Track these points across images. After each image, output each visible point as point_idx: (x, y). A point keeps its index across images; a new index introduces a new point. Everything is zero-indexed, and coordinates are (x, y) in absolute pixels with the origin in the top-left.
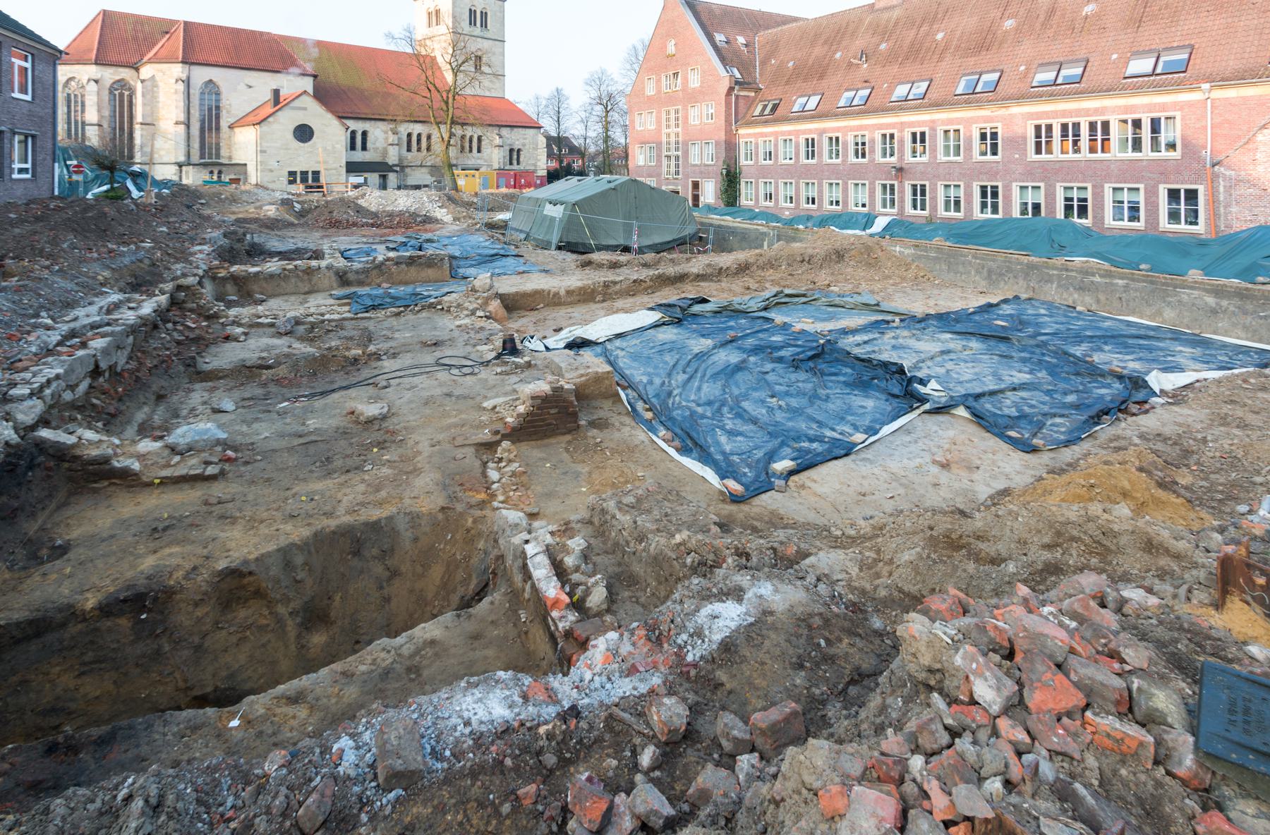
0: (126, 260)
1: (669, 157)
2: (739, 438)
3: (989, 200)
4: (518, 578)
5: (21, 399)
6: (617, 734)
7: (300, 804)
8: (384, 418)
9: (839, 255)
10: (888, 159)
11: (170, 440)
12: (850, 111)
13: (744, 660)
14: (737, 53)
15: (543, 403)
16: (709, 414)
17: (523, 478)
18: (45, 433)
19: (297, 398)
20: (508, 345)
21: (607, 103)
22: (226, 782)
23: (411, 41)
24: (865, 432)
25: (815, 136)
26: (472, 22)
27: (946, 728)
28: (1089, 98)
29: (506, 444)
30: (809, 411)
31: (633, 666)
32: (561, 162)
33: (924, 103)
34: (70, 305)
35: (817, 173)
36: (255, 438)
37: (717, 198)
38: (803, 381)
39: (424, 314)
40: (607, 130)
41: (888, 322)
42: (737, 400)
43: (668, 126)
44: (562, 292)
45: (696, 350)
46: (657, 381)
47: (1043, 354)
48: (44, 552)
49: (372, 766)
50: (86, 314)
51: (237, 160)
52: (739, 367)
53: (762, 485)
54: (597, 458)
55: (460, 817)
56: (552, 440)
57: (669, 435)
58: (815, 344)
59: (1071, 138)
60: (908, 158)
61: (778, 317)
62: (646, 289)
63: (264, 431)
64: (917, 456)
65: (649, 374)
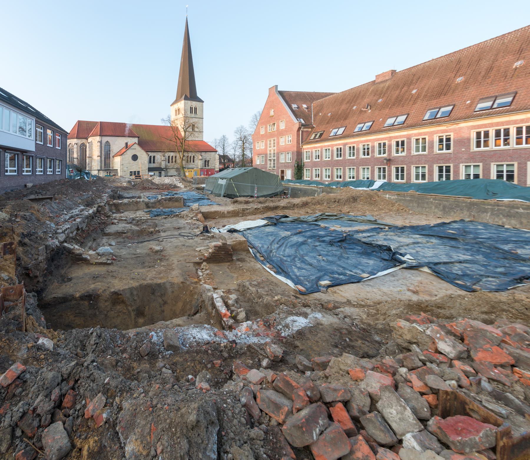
0: (85, 197)
1: (270, 160)
2: (303, 271)
3: (444, 173)
4: (210, 308)
5: (60, 233)
6: (252, 353)
7: (140, 347)
8: (161, 251)
9: (354, 199)
10: (382, 155)
11: (98, 251)
12: (361, 134)
13: (308, 339)
14: (303, 112)
15: (219, 249)
16: (289, 260)
17: (212, 276)
18: (65, 244)
19: (134, 243)
20: (205, 229)
21: (244, 140)
22: (118, 336)
23: (169, 120)
24: (369, 273)
25: (342, 147)
26: (191, 112)
27: (420, 360)
28: (517, 114)
29: (204, 263)
30: (339, 263)
31: (258, 333)
32: (225, 165)
33: (404, 126)
34: (71, 209)
35: (343, 164)
36: (121, 254)
37: (292, 177)
38: (335, 250)
39: (175, 218)
40: (244, 151)
41: (381, 229)
42: (302, 256)
43: (270, 147)
44: (226, 212)
45: (283, 236)
46: (266, 246)
47: (481, 248)
48: (66, 280)
49: (162, 342)
50: (76, 211)
51: (115, 168)
52: (303, 243)
53: (315, 289)
54: (240, 272)
55: (193, 365)
56: (222, 264)
57: (271, 266)
58: (341, 236)
59: (502, 137)
60: (394, 154)
61: (322, 224)
62: (260, 212)
63: (124, 252)
64: (399, 286)
65: (262, 244)
